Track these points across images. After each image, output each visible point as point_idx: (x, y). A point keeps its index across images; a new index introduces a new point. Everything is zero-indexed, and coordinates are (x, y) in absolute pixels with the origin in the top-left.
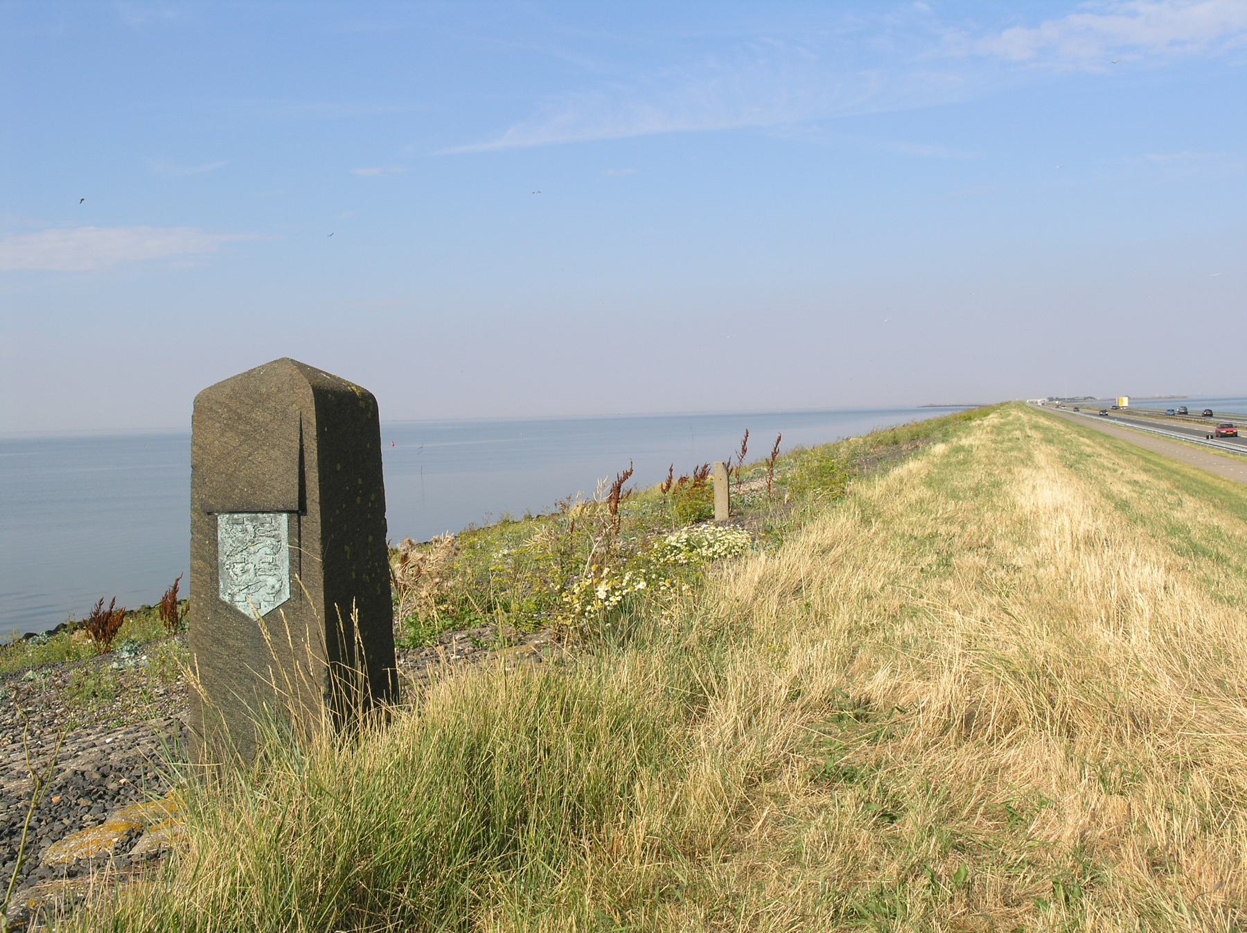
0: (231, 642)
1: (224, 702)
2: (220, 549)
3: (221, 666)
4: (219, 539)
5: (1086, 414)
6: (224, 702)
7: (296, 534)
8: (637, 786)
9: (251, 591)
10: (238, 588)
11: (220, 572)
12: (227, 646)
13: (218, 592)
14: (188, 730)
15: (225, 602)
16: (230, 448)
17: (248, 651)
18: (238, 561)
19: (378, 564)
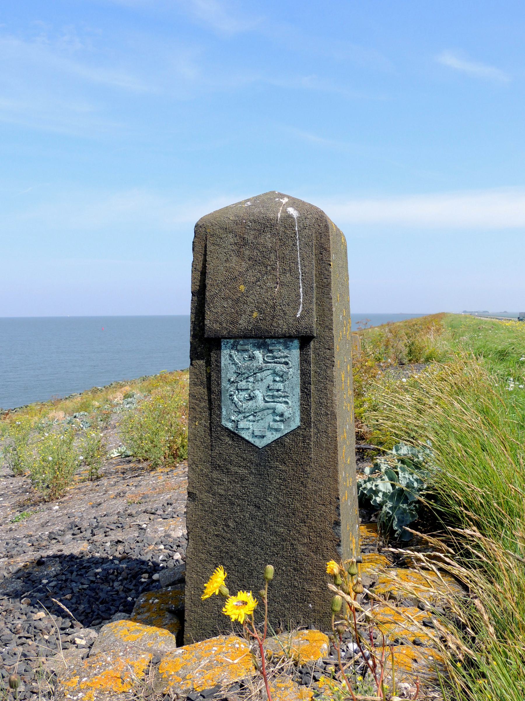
0: (234, 469)
1: (225, 528)
2: (223, 375)
3: (223, 492)
4: (222, 365)
5: (449, 564)
6: (225, 528)
7: (347, 308)
8: (35, 552)
9: (257, 418)
10: (243, 415)
11: (223, 398)
12: (228, 472)
13: (220, 418)
14: (316, 249)
15: (227, 429)
16: (237, 273)
17: (251, 478)
18: (243, 388)
19: (170, 591)
